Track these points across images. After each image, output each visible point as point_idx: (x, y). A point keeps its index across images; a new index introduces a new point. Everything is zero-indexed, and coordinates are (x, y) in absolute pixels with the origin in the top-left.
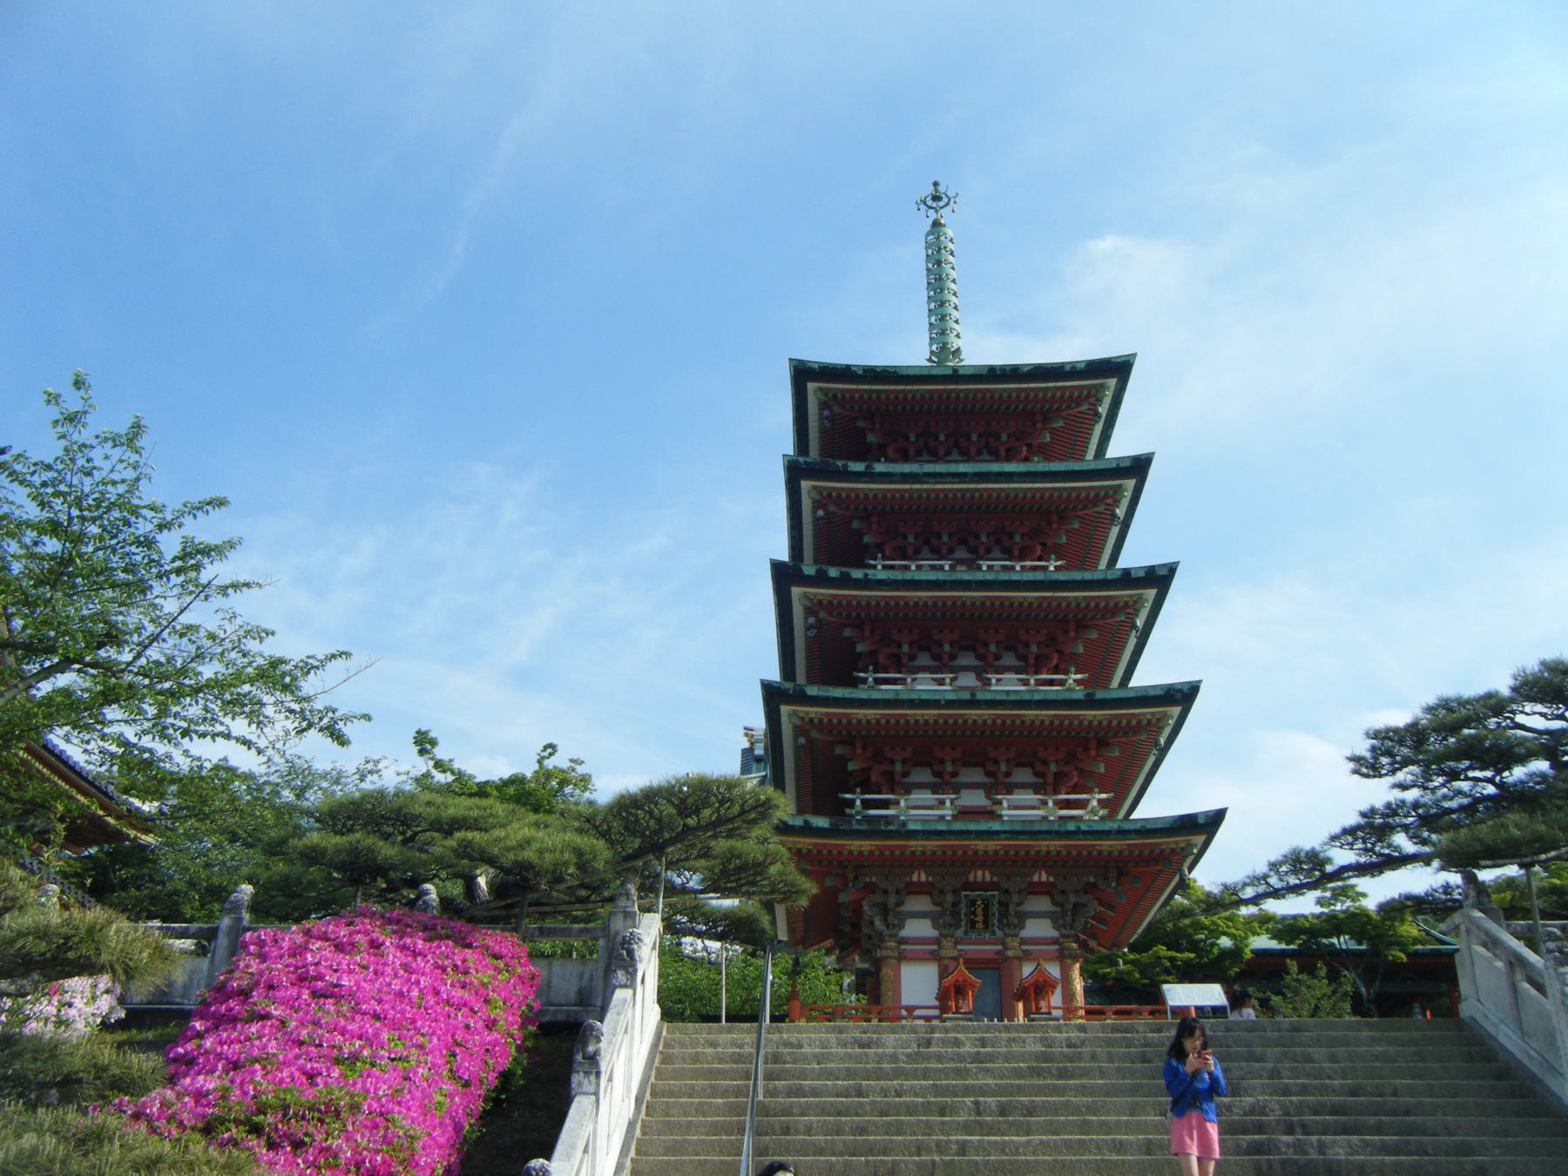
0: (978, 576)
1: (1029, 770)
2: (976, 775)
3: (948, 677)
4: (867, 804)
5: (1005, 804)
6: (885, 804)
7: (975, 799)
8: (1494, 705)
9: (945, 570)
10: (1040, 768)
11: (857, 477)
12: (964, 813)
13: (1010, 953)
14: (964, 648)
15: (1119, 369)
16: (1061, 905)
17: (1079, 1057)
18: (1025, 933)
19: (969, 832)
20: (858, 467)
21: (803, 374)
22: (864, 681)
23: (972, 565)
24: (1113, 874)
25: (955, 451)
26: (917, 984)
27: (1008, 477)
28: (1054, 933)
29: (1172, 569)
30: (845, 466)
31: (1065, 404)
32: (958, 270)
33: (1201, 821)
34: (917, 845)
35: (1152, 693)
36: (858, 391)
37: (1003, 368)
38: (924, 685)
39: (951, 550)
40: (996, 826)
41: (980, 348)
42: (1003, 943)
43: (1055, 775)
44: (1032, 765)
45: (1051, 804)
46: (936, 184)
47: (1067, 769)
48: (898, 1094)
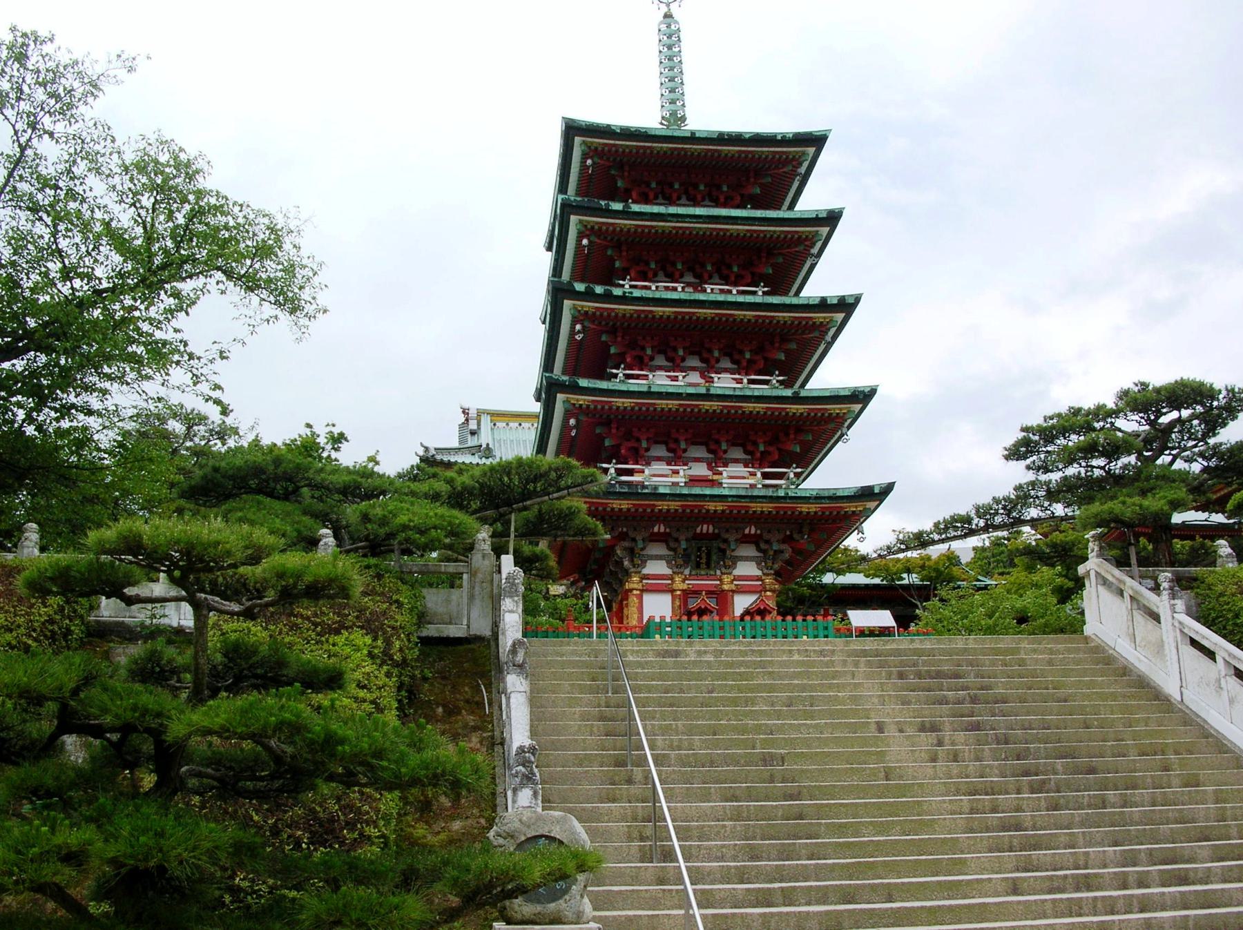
0: (702, 297)
1: (704, 448)
2: (700, 452)
3: (680, 375)
4: (620, 472)
5: (725, 474)
6: (630, 472)
7: (701, 470)
8: (1100, 412)
9: (680, 292)
10: (750, 448)
11: (616, 214)
12: (693, 481)
13: (726, 587)
14: (692, 353)
15: (817, 141)
16: (674, 550)
18: (645, 571)
19: (705, 496)
20: (617, 206)
21: (572, 130)
22: (616, 376)
23: (699, 288)
24: (806, 529)
25: (684, 197)
26: (658, 607)
27: (734, 220)
28: (759, 573)
30: (608, 205)
31: (768, 166)
33: (877, 490)
34: (663, 505)
35: (842, 393)
36: (614, 145)
37: (729, 134)
38: (660, 381)
39: (682, 276)
40: (716, 491)
41: (710, 114)
42: (720, 580)
43: (762, 453)
44: (666, 443)
45: (759, 475)
48: (681, 691)
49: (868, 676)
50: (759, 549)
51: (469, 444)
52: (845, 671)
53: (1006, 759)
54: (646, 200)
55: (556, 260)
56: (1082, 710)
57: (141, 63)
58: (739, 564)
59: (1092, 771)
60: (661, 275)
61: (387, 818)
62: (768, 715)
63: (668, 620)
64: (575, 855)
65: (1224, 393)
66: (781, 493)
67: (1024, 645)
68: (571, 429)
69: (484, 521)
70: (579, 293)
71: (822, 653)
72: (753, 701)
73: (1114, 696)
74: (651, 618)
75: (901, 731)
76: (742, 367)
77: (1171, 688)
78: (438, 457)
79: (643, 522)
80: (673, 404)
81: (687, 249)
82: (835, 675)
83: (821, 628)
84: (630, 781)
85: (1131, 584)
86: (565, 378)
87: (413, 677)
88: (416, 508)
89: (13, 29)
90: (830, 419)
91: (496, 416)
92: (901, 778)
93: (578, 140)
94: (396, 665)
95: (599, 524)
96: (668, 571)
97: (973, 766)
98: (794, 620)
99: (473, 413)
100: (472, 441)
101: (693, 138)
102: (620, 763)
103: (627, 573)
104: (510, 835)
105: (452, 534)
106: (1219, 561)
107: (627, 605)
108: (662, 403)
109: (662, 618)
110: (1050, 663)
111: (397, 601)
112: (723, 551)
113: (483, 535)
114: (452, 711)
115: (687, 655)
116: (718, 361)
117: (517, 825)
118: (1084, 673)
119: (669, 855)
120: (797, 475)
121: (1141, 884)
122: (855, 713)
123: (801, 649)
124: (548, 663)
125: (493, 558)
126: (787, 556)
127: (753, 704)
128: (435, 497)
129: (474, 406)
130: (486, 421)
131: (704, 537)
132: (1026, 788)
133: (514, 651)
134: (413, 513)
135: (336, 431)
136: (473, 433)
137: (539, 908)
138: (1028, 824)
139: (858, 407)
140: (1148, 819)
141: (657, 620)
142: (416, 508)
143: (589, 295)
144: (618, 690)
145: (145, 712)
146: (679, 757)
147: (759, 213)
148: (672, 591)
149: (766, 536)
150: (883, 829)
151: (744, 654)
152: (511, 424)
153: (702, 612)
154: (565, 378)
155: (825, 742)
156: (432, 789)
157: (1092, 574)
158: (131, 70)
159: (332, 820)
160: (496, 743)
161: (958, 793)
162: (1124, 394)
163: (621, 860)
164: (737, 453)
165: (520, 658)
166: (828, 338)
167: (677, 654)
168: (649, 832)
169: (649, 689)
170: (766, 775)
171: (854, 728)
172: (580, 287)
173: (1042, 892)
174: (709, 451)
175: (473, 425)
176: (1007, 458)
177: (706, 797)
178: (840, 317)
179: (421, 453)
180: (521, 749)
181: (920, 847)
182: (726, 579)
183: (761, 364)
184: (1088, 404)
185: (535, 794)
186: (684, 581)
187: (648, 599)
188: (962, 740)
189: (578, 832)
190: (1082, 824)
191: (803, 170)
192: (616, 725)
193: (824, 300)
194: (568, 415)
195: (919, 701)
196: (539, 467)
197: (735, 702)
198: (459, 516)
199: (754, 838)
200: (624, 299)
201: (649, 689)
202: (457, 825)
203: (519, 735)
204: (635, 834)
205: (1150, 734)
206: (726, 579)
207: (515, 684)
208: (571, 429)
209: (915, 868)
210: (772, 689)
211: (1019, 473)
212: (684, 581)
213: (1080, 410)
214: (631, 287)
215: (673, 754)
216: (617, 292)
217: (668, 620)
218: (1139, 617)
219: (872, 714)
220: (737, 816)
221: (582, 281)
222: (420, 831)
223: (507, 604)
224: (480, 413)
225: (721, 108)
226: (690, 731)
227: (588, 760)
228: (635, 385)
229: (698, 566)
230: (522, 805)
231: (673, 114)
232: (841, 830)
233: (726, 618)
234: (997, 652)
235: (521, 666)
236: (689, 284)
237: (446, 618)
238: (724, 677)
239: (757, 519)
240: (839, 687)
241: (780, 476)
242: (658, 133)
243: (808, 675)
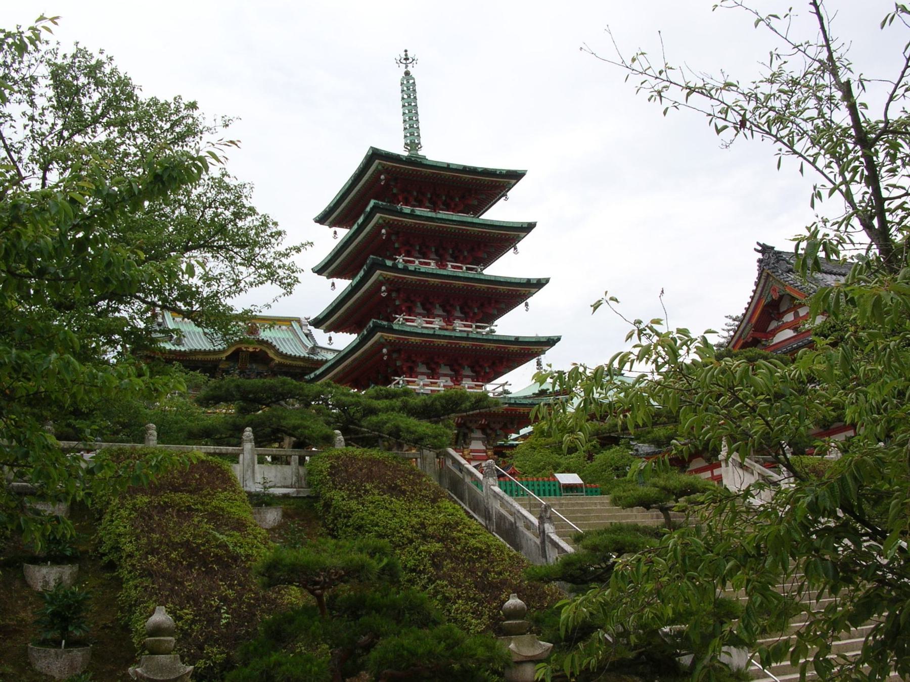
15: (516, 176)
28: (484, 448)
30: (413, 211)
37: (470, 168)
41: (439, 149)
46: (406, 51)
55: (350, 237)
58: (473, 442)
70: (411, 271)
80: (418, 339)
89: (758, 243)
108: (413, 339)
149: (492, 425)
174: (452, 370)
193: (529, 280)
208: (384, 355)
214: (421, 263)
225: (447, 145)
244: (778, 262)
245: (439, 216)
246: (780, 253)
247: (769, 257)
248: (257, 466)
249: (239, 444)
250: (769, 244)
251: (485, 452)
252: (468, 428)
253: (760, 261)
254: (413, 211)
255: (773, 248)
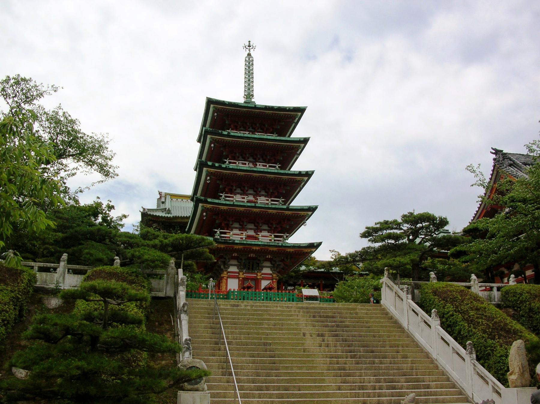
1: (253, 225)
2: (252, 226)
3: (246, 197)
4: (221, 233)
5: (260, 235)
6: (225, 233)
7: (251, 233)
11: (224, 136)
12: (249, 237)
13: (258, 277)
15: (301, 111)
16: (274, 265)
17: (290, 311)
18: (229, 270)
21: (210, 102)
26: (233, 284)
28: (271, 272)
29: (313, 172)
31: (284, 119)
32: (481, 380)
33: (315, 245)
34: (236, 247)
37: (269, 107)
41: (263, 98)
45: (273, 236)
46: (249, 42)
47: (278, 226)
48: (238, 319)
49: (303, 316)
50: (271, 264)
51: (161, 208)
52: (296, 315)
53: (345, 347)
54: (236, 129)
56: (373, 331)
57: (60, 90)
58: (231, 267)
59: (372, 352)
60: (240, 158)
61: (144, 359)
62: (267, 329)
63: (236, 290)
64: (204, 371)
65: (438, 219)
66: (280, 244)
67: (359, 307)
68: (204, 216)
69: (172, 256)
71: (288, 307)
72: (262, 324)
73: (386, 327)
74: (230, 290)
75: (311, 336)
76: (269, 195)
77: (405, 324)
78: (149, 213)
79: (228, 252)
81: (250, 145)
82: (291, 316)
83: (291, 295)
84: (219, 350)
85: (396, 287)
86: (203, 198)
87: (148, 312)
88: (150, 252)
90: (300, 217)
91: (173, 196)
92: (309, 352)
93: (212, 106)
94: (144, 308)
95: (213, 257)
96: (237, 270)
97: (333, 349)
98: (282, 292)
99: (163, 194)
100: (162, 206)
101: (255, 107)
102: (216, 343)
103: (222, 271)
104: (185, 366)
105: (162, 262)
106: (431, 279)
107: (222, 282)
109: (234, 290)
110: (366, 314)
111: (143, 286)
112: (258, 264)
113: (172, 261)
114: (161, 324)
115: (241, 306)
116: (260, 192)
117: (187, 363)
118: (377, 318)
119: (231, 374)
120: (287, 236)
121: (380, 389)
122: (296, 329)
123: (281, 307)
124: (193, 307)
125: (175, 269)
126: (282, 267)
127: (263, 325)
128: (154, 246)
129: (164, 191)
130: (168, 198)
131: (250, 259)
132: (349, 357)
133: (184, 306)
134: (149, 254)
135: (111, 204)
136: (163, 203)
137: (192, 387)
138: (348, 368)
139: (310, 213)
140: (387, 368)
141: (232, 290)
142: (150, 252)
143: (213, 166)
144: (217, 318)
145: (94, 331)
146: (236, 343)
147: (278, 138)
148: (239, 278)
150: (300, 368)
151: (260, 306)
152: (179, 200)
153: (249, 288)
154: (203, 198)
155: (285, 339)
156: (154, 351)
157: (384, 283)
158: (55, 91)
159: (129, 360)
160: (176, 335)
161: (327, 357)
162: (404, 216)
163: (216, 374)
164: (265, 227)
165: (185, 309)
166: (301, 186)
167: (238, 306)
168: (225, 366)
169: (227, 318)
170: (264, 349)
171: (295, 334)
172: (210, 163)
173: (348, 390)
175: (163, 200)
176: (361, 237)
177: (244, 356)
178: (306, 178)
179: (142, 211)
180: (186, 340)
181: (311, 374)
182: (259, 274)
183: (276, 194)
184: (390, 219)
185: (190, 354)
186: (243, 274)
187: (230, 280)
188: (331, 340)
189: (203, 365)
190: (365, 369)
191: (296, 121)
192: (216, 331)
193: (300, 172)
194: (202, 211)
195: (319, 326)
196: (193, 239)
197: (256, 324)
198: (165, 256)
199: (258, 370)
200: (226, 169)
201: (227, 318)
202: (164, 362)
203: (185, 336)
204: (220, 367)
205: (395, 340)
206: (259, 274)
207: (184, 317)
208: (204, 216)
209: (308, 381)
210: (269, 320)
211: (365, 243)
212: (243, 274)
213: (388, 221)
215: (234, 341)
216: (224, 166)
217: (236, 290)
218: (397, 298)
219: (302, 330)
220: (254, 362)
221: (210, 161)
222: (152, 364)
223: (181, 288)
224: (166, 194)
225: (266, 96)
226: (240, 333)
227: (206, 342)
228: (232, 166)
229: (249, 269)
230: (186, 358)
231: (249, 94)
232: (287, 368)
233: (257, 291)
234: (348, 309)
235: (186, 311)
236: (250, 162)
237: (158, 290)
238: (254, 315)
239: (271, 253)
240: (292, 320)
241: (281, 237)
242: (242, 105)
243: (282, 315)
244: (504, 160)
245: (255, 136)
246: (506, 154)
247: (501, 158)
248: (66, 275)
249: (58, 261)
250: (499, 148)
251: (239, 273)
252: (259, 260)
253: (494, 159)
254: (229, 133)
255: (502, 151)
